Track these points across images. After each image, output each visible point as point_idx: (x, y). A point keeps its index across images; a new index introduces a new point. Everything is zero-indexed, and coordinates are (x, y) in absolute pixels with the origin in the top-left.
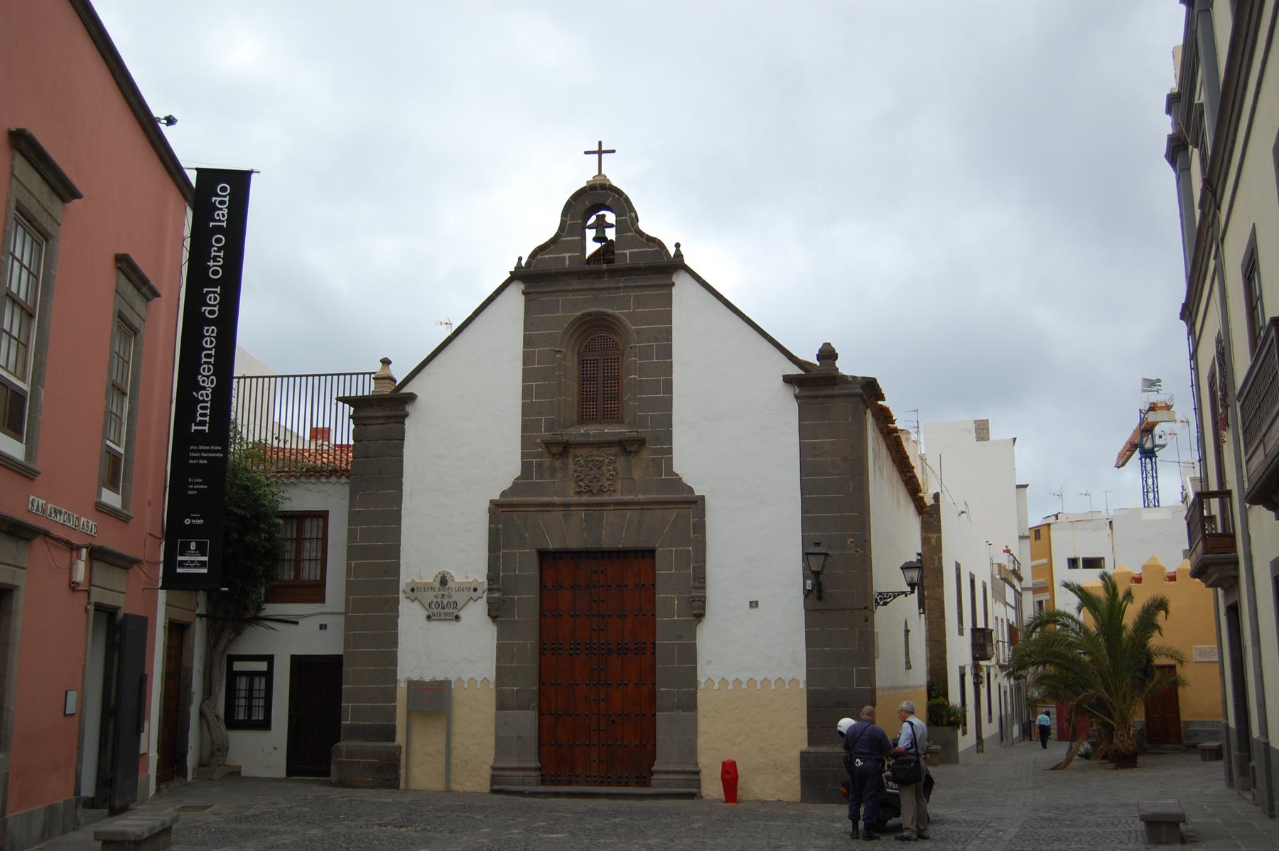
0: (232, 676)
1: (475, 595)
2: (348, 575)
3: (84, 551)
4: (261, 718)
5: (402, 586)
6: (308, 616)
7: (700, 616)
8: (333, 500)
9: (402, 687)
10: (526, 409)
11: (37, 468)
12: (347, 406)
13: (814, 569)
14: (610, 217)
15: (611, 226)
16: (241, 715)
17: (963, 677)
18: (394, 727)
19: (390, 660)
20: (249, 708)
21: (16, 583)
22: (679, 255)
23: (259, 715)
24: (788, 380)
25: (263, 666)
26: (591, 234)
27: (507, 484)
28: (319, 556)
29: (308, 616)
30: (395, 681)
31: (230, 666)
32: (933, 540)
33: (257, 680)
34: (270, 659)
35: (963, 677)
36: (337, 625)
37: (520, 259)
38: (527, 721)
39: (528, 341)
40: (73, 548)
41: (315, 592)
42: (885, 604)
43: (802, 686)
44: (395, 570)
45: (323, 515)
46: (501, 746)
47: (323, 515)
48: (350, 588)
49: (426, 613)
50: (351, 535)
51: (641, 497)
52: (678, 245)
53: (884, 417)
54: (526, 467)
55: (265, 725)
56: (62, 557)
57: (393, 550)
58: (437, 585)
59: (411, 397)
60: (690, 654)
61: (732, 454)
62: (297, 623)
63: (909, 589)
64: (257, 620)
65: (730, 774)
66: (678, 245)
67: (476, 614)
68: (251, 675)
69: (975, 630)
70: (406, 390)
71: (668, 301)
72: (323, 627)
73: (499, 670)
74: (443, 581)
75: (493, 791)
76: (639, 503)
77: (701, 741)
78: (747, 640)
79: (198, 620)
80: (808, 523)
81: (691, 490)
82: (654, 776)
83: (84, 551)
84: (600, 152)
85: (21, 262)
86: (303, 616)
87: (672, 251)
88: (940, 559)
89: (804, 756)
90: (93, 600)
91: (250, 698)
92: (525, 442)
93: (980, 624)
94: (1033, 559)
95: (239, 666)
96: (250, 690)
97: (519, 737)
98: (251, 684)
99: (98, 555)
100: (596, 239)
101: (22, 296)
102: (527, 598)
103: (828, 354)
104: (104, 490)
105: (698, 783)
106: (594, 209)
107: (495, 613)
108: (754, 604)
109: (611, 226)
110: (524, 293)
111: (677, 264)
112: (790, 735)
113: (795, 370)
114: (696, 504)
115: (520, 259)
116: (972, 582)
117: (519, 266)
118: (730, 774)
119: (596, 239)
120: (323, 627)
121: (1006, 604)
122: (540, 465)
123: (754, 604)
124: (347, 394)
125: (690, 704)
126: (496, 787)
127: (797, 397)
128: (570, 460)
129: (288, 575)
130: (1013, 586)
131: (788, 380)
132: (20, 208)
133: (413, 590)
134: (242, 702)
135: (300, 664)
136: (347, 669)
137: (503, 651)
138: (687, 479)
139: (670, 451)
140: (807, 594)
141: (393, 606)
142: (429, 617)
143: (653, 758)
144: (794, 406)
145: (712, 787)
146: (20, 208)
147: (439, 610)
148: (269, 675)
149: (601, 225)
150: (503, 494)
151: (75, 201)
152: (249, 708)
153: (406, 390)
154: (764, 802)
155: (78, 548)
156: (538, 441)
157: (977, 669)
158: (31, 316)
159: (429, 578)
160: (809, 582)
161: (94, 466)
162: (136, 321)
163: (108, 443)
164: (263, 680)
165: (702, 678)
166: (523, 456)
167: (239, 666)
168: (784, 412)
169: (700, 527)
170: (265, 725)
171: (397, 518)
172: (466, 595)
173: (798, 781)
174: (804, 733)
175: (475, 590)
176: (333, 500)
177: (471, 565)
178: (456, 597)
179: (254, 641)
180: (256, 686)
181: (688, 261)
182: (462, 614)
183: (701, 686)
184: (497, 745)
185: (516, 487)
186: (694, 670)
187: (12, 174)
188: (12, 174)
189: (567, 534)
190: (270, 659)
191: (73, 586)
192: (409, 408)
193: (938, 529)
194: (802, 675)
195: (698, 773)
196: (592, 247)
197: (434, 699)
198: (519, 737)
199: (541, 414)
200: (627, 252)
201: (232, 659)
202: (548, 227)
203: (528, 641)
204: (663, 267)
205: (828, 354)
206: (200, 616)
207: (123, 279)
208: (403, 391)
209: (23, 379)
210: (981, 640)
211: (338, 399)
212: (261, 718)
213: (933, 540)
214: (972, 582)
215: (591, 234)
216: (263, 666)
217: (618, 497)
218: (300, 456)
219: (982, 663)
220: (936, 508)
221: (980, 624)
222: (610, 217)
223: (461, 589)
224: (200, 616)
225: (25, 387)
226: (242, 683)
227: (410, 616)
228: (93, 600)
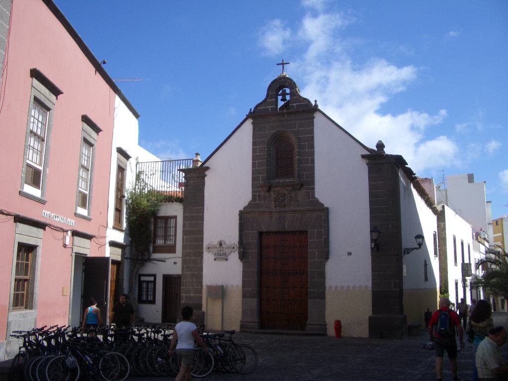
0: (141, 283)
1: (233, 250)
2: (183, 242)
3: (69, 232)
4: (152, 299)
5: (205, 246)
6: (169, 258)
7: (327, 258)
8: (175, 210)
9: (204, 287)
10: (254, 172)
11: (46, 200)
12: (181, 172)
13: (374, 238)
14: (288, 91)
15: (288, 94)
16: (144, 298)
17: (457, 284)
18: (201, 304)
19: (199, 277)
20: (147, 295)
21: (37, 244)
22: (316, 106)
23: (150, 298)
24: (363, 157)
25: (152, 279)
26: (280, 98)
27: (246, 204)
28: (163, 234)
29: (169, 258)
30: (202, 286)
31: (140, 279)
32: (442, 226)
33: (150, 284)
34: (155, 276)
35: (457, 284)
36: (179, 262)
37: (251, 109)
38: (254, 302)
39: (254, 144)
40: (67, 231)
41: (172, 249)
42: (408, 253)
43: (370, 288)
44: (202, 240)
45: (175, 217)
46: (244, 312)
47: (175, 217)
48: (184, 247)
49: (214, 257)
50: (184, 226)
51: (301, 208)
52: (316, 101)
53: (409, 173)
54: (254, 196)
55: (153, 302)
56: (61, 234)
57: (201, 232)
58: (218, 246)
59: (208, 168)
60: (322, 275)
61: (341, 192)
62: (165, 261)
63: (418, 246)
64: (149, 260)
65: (338, 325)
66: (316, 101)
67: (234, 257)
68: (148, 282)
69: (463, 264)
70: (206, 165)
71: (312, 124)
72: (175, 263)
73: (243, 281)
74: (221, 244)
75: (241, 331)
76: (300, 211)
77: (327, 311)
78: (348, 268)
79: (125, 260)
80: (372, 219)
81: (322, 205)
82: (308, 326)
83: (69, 232)
84: (283, 64)
85: (38, 120)
86: (167, 259)
87: (313, 103)
88: (445, 234)
89: (370, 318)
90: (74, 251)
91: (148, 291)
92: (253, 186)
93: (466, 261)
94: (494, 234)
95: (143, 278)
96: (148, 288)
97: (252, 309)
98: (148, 286)
99: (75, 233)
100: (282, 100)
101: (39, 133)
102: (254, 251)
103: (380, 146)
104: (78, 207)
105: (326, 330)
106: (281, 87)
107: (243, 256)
108: (349, 254)
109: (288, 94)
110: (252, 123)
111: (315, 109)
112: (365, 309)
113: (366, 153)
114: (326, 211)
115: (251, 109)
116: (462, 243)
117: (250, 112)
118: (338, 325)
119: (282, 100)
120: (175, 263)
121: (480, 252)
122: (259, 196)
123: (349, 254)
124: (181, 168)
125: (322, 296)
126: (242, 330)
127: (367, 164)
128: (272, 193)
129: (160, 242)
130: (484, 245)
131: (363, 157)
132: (36, 100)
133: (208, 248)
134: (144, 293)
135: (167, 279)
136: (183, 280)
137: (245, 274)
138: (322, 200)
139: (314, 188)
140: (372, 249)
141: (201, 254)
142: (215, 259)
143: (306, 319)
144: (366, 168)
145: (331, 332)
146: (36, 100)
147: (219, 256)
148: (154, 282)
149: (284, 94)
150: (245, 208)
151: (60, 95)
152: (147, 295)
153: (206, 165)
154: (353, 338)
155: (67, 231)
156: (258, 185)
157: (464, 281)
158: (43, 140)
159: (215, 242)
160: (373, 244)
161: (74, 198)
162: (92, 141)
163: (80, 189)
164: (152, 284)
165: (327, 285)
166: (253, 192)
167: (143, 278)
168: (363, 170)
169: (327, 221)
170: (153, 302)
171: (202, 218)
172: (229, 250)
173: (368, 329)
174: (371, 308)
175: (233, 248)
176: (175, 210)
177: (232, 236)
178: (226, 251)
179: (149, 268)
180: (150, 287)
181: (320, 107)
182: (229, 258)
183: (327, 289)
184: (243, 312)
185: (250, 205)
186: (324, 282)
187: (32, 86)
188: (32, 86)
189: (269, 224)
190: (155, 276)
191: (65, 246)
192: (207, 173)
193: (444, 221)
194: (369, 284)
195: (326, 325)
196: (281, 104)
197: (220, 292)
198: (252, 309)
199: (259, 174)
200: (295, 104)
201: (140, 275)
202: (261, 96)
203: (254, 270)
204: (309, 110)
205: (380, 146)
206: (127, 258)
207: (120, 155)
208: (204, 166)
209: (40, 165)
210: (466, 269)
211: (178, 170)
212: (152, 299)
213: (442, 226)
214: (462, 243)
215: (280, 98)
216: (152, 279)
217: (292, 208)
218: (175, 194)
219: (467, 278)
220: (443, 212)
221: (466, 261)
222: (288, 91)
223: (228, 248)
224: (127, 258)
225: (41, 168)
226: (145, 285)
227: (208, 258)
228: (74, 251)
